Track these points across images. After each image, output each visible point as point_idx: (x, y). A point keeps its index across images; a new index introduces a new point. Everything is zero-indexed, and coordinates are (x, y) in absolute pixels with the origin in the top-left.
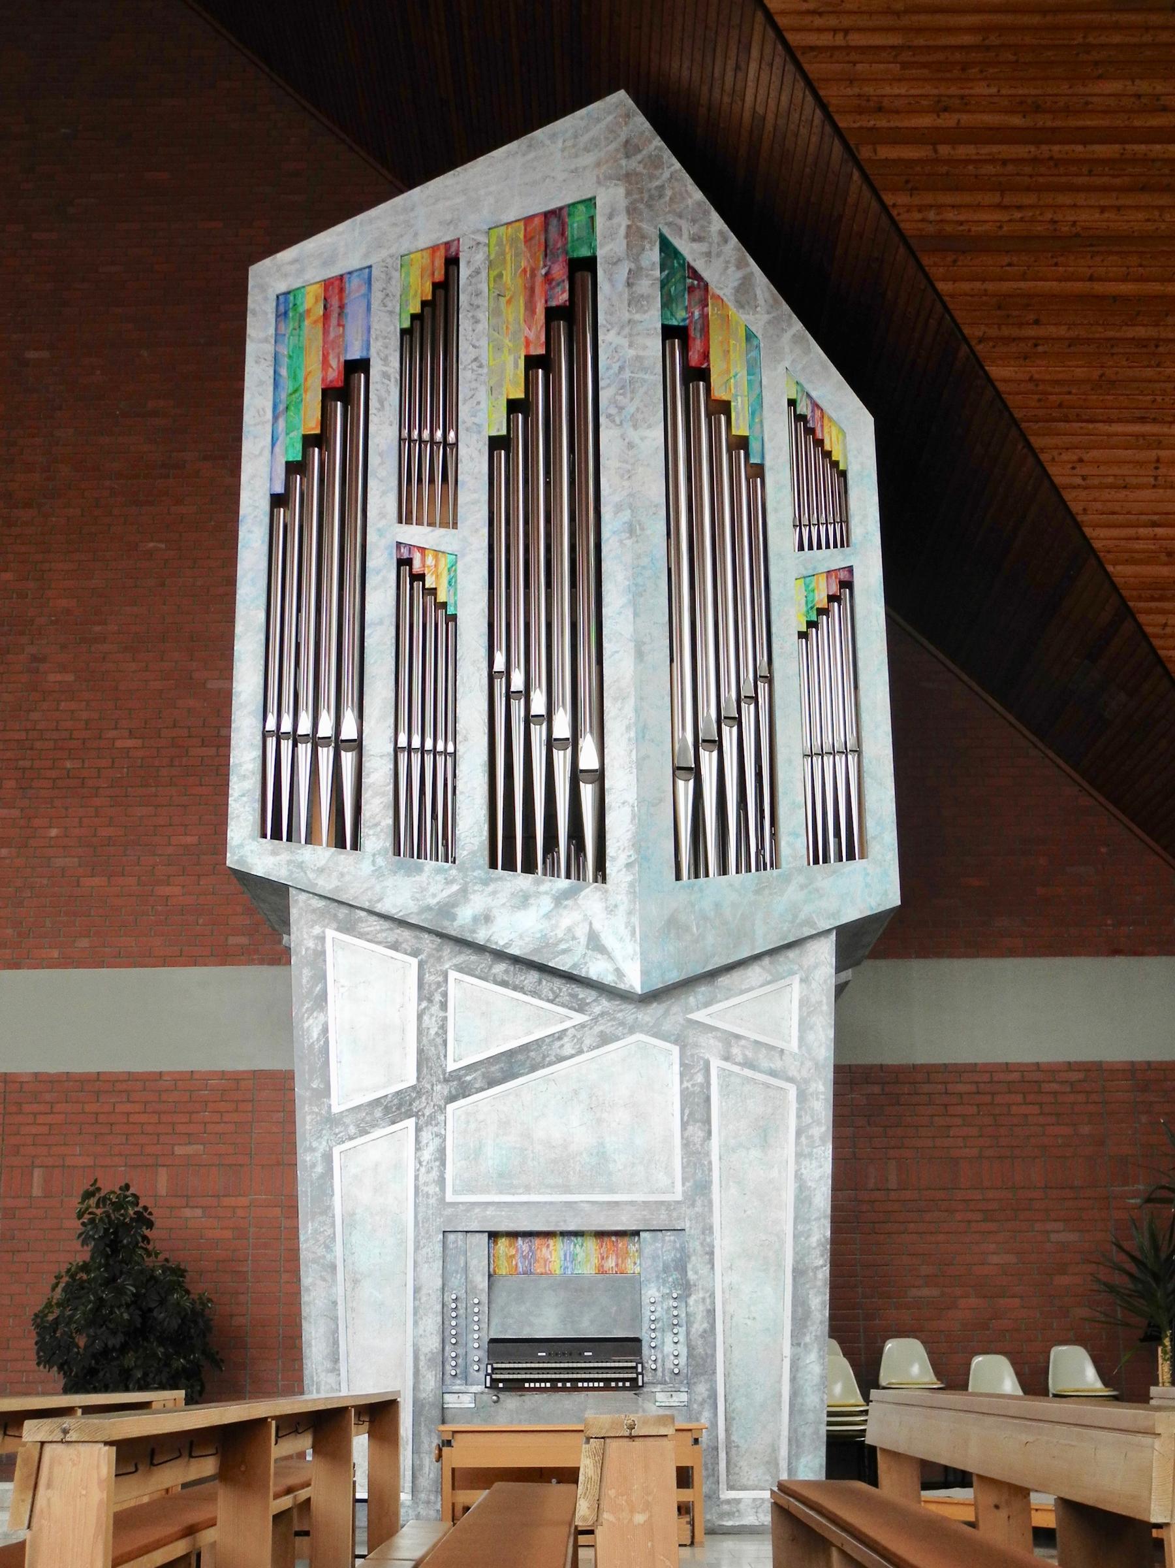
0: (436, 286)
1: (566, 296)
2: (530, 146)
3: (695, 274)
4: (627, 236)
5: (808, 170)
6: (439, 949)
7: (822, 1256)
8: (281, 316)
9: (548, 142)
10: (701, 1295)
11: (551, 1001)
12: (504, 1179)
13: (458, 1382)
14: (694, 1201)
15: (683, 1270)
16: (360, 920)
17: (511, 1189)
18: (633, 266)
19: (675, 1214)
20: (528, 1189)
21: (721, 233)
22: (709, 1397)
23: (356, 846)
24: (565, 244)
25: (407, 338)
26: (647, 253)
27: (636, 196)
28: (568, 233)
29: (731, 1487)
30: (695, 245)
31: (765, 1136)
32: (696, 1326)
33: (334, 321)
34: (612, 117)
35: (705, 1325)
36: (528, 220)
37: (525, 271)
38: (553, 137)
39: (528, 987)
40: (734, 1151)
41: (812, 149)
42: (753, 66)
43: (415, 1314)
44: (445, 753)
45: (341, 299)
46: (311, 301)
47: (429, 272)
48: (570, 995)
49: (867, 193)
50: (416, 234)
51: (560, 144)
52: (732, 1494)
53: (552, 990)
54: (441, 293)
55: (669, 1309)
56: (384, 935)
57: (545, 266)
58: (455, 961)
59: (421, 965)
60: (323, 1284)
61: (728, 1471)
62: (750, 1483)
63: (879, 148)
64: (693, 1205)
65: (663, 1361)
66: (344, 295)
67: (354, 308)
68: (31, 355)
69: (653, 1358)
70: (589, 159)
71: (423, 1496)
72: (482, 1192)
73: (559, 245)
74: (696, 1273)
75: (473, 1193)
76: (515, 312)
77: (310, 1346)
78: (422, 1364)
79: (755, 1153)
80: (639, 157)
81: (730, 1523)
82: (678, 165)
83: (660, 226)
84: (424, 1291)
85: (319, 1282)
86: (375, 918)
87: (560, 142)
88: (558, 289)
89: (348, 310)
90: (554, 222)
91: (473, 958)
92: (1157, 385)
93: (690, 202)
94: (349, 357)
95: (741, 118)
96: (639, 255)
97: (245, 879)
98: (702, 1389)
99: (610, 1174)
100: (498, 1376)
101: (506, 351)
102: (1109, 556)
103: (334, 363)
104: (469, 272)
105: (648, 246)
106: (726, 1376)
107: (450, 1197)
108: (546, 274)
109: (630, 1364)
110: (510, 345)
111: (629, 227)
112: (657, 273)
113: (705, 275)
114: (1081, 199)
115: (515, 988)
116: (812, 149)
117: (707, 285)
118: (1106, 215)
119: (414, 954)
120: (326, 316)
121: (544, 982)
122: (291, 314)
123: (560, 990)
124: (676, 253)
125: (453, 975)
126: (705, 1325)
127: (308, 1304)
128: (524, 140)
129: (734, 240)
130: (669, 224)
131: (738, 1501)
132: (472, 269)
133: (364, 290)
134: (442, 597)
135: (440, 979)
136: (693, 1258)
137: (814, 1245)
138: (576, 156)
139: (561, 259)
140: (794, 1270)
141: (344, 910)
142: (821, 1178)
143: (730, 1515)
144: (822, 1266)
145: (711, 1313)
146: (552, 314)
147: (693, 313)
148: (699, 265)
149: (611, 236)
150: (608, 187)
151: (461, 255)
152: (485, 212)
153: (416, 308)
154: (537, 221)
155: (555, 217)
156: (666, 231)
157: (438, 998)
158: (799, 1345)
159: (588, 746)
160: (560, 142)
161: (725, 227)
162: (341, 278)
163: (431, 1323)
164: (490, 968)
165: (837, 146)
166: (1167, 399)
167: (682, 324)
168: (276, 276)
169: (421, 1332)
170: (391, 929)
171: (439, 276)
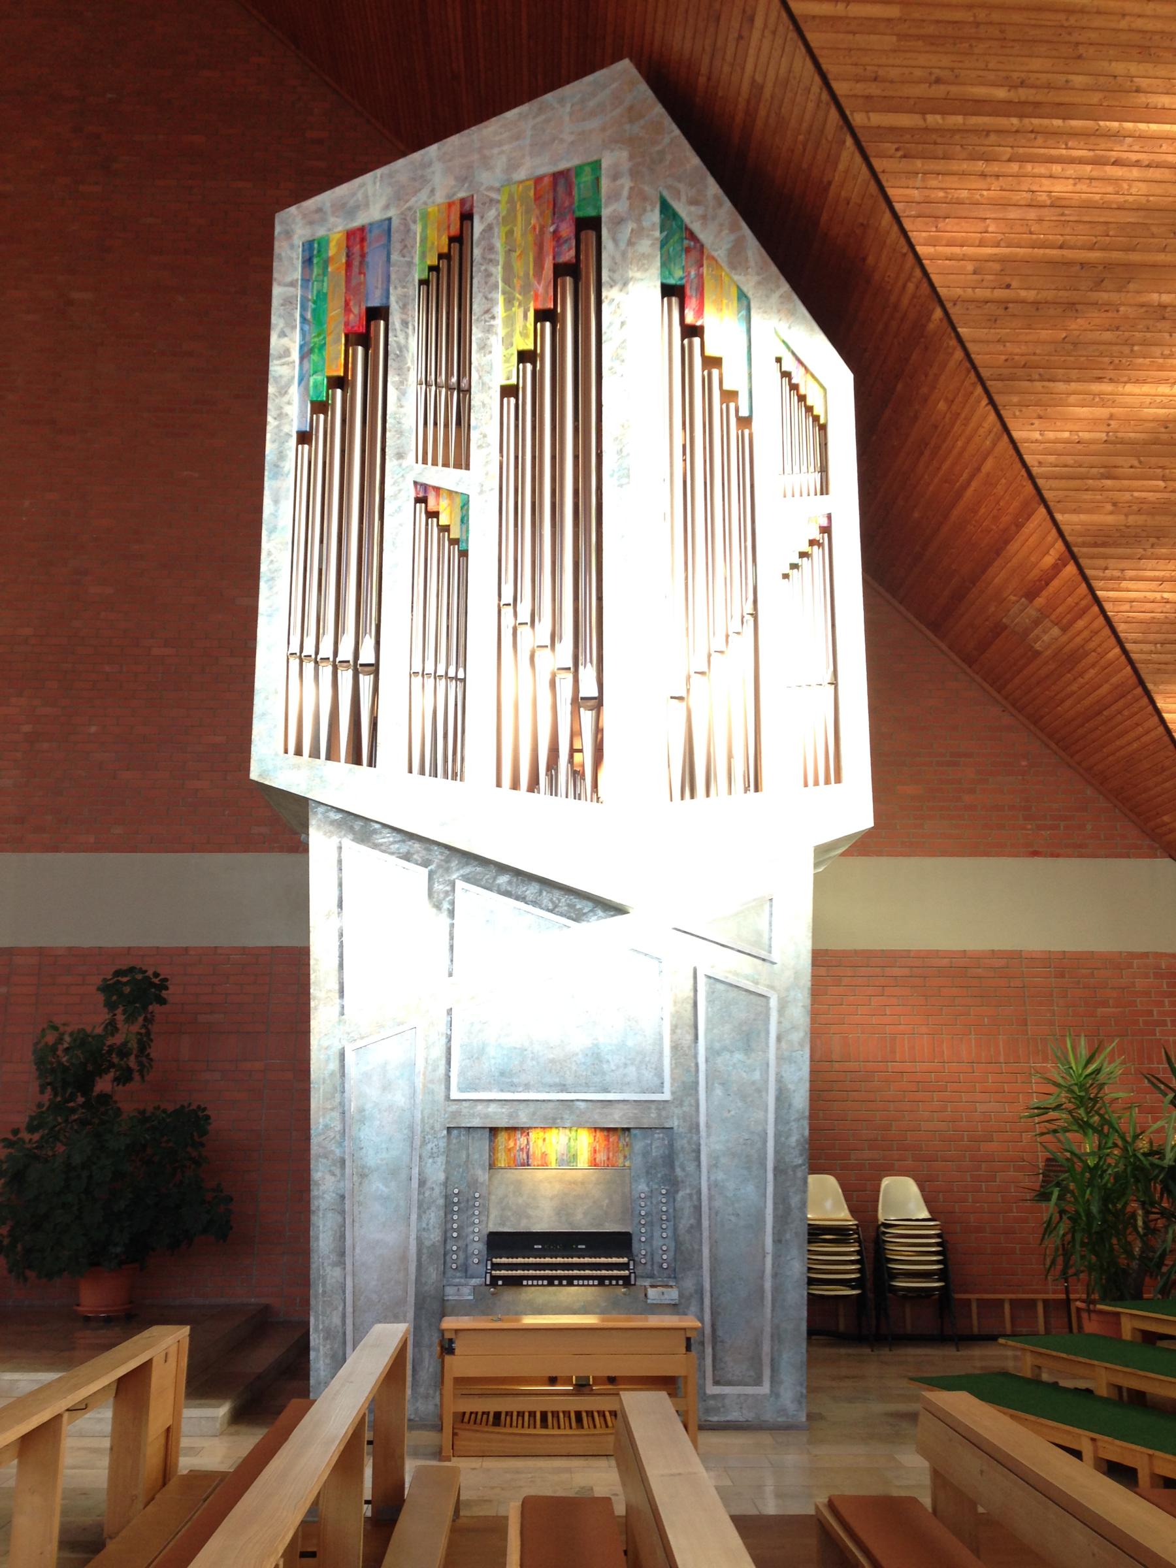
0: (452, 240)
1: (573, 253)
2: (540, 109)
3: (692, 236)
4: (629, 198)
5: (801, 138)
6: (447, 861)
7: (801, 1155)
8: (308, 262)
9: (556, 105)
10: (688, 1191)
11: (551, 911)
12: (505, 1078)
13: (458, 1274)
14: (682, 1101)
15: (672, 1167)
16: (375, 832)
17: (513, 1087)
18: (635, 226)
19: (664, 1113)
20: (527, 1087)
21: (716, 197)
22: (696, 1291)
23: (372, 763)
24: (572, 203)
25: (424, 288)
26: (649, 214)
27: (639, 160)
28: (575, 192)
29: (717, 1383)
30: (693, 208)
31: (748, 1040)
32: (683, 1221)
33: (355, 269)
34: (621, 77)
35: (692, 1221)
36: (538, 180)
37: (534, 228)
38: (562, 101)
39: (530, 898)
40: (718, 1053)
41: (808, 116)
42: (756, 34)
43: (419, 1207)
44: (456, 678)
45: (362, 248)
46: (335, 248)
47: (445, 226)
48: (568, 905)
49: (858, 159)
50: (433, 191)
51: (568, 108)
52: (717, 1390)
53: (551, 900)
54: (456, 246)
55: (658, 1204)
56: (397, 846)
57: (553, 223)
58: (462, 872)
59: (431, 874)
60: (333, 1179)
61: (714, 1366)
62: (735, 1378)
63: (871, 115)
64: (681, 1105)
65: (652, 1254)
66: (365, 244)
67: (375, 258)
68: (76, 295)
69: (643, 1252)
70: (594, 124)
71: (422, 1390)
72: (484, 1089)
73: (567, 204)
74: (683, 1170)
75: (476, 1090)
76: (523, 266)
77: (317, 1239)
78: (424, 1257)
79: (738, 1056)
80: (642, 122)
81: (715, 1419)
82: (677, 132)
83: (661, 188)
84: (429, 1184)
85: (328, 1177)
86: (388, 830)
87: (568, 106)
88: (565, 247)
89: (369, 259)
90: (562, 182)
91: (478, 869)
92: (1115, 348)
93: (688, 167)
94: (370, 305)
95: (740, 87)
96: (640, 215)
97: (621, 58)
98: (689, 1284)
99: (604, 1073)
100: (498, 1272)
101: (516, 304)
102: (1059, 505)
103: (356, 310)
104: (482, 228)
105: (649, 208)
106: (713, 1271)
107: (455, 1095)
108: (555, 232)
109: (621, 1260)
110: (520, 297)
111: (631, 188)
112: (657, 234)
113: (702, 236)
114: (1056, 169)
115: (517, 898)
116: (808, 116)
117: (702, 246)
118: (1079, 187)
119: (425, 864)
120: (349, 265)
121: (544, 893)
122: (315, 261)
123: (559, 900)
124: (675, 215)
125: (460, 884)
126: (692, 1221)
127: (318, 1197)
128: (536, 103)
129: (728, 204)
130: (669, 187)
131: (722, 1397)
132: (485, 224)
133: (384, 241)
134: (454, 534)
135: (448, 888)
136: (681, 1155)
137: (794, 1144)
138: (584, 120)
139: (568, 217)
140: (775, 1169)
141: (359, 827)
142: (801, 1079)
143: (716, 1410)
144: (801, 1165)
145: (698, 1209)
146: (560, 270)
147: (689, 273)
148: (696, 227)
149: (615, 196)
150: (612, 150)
151: (475, 210)
152: (498, 170)
153: (432, 260)
154: (546, 181)
155: (561, 178)
156: (666, 194)
157: (446, 906)
158: (780, 1241)
159: (588, 674)
160: (568, 106)
161: (720, 192)
162: (362, 229)
163: (434, 1217)
164: (495, 878)
165: (834, 114)
166: (1124, 360)
167: (679, 283)
168: (301, 227)
169: (424, 1225)
170: (403, 841)
171: (455, 230)
